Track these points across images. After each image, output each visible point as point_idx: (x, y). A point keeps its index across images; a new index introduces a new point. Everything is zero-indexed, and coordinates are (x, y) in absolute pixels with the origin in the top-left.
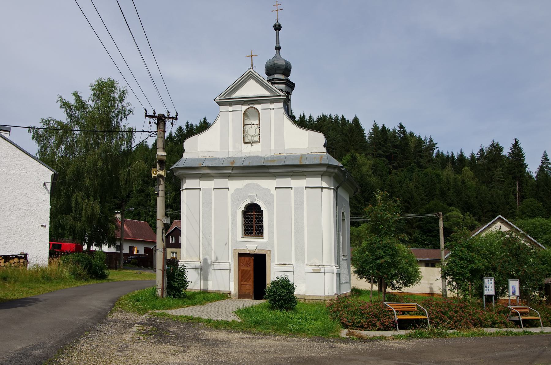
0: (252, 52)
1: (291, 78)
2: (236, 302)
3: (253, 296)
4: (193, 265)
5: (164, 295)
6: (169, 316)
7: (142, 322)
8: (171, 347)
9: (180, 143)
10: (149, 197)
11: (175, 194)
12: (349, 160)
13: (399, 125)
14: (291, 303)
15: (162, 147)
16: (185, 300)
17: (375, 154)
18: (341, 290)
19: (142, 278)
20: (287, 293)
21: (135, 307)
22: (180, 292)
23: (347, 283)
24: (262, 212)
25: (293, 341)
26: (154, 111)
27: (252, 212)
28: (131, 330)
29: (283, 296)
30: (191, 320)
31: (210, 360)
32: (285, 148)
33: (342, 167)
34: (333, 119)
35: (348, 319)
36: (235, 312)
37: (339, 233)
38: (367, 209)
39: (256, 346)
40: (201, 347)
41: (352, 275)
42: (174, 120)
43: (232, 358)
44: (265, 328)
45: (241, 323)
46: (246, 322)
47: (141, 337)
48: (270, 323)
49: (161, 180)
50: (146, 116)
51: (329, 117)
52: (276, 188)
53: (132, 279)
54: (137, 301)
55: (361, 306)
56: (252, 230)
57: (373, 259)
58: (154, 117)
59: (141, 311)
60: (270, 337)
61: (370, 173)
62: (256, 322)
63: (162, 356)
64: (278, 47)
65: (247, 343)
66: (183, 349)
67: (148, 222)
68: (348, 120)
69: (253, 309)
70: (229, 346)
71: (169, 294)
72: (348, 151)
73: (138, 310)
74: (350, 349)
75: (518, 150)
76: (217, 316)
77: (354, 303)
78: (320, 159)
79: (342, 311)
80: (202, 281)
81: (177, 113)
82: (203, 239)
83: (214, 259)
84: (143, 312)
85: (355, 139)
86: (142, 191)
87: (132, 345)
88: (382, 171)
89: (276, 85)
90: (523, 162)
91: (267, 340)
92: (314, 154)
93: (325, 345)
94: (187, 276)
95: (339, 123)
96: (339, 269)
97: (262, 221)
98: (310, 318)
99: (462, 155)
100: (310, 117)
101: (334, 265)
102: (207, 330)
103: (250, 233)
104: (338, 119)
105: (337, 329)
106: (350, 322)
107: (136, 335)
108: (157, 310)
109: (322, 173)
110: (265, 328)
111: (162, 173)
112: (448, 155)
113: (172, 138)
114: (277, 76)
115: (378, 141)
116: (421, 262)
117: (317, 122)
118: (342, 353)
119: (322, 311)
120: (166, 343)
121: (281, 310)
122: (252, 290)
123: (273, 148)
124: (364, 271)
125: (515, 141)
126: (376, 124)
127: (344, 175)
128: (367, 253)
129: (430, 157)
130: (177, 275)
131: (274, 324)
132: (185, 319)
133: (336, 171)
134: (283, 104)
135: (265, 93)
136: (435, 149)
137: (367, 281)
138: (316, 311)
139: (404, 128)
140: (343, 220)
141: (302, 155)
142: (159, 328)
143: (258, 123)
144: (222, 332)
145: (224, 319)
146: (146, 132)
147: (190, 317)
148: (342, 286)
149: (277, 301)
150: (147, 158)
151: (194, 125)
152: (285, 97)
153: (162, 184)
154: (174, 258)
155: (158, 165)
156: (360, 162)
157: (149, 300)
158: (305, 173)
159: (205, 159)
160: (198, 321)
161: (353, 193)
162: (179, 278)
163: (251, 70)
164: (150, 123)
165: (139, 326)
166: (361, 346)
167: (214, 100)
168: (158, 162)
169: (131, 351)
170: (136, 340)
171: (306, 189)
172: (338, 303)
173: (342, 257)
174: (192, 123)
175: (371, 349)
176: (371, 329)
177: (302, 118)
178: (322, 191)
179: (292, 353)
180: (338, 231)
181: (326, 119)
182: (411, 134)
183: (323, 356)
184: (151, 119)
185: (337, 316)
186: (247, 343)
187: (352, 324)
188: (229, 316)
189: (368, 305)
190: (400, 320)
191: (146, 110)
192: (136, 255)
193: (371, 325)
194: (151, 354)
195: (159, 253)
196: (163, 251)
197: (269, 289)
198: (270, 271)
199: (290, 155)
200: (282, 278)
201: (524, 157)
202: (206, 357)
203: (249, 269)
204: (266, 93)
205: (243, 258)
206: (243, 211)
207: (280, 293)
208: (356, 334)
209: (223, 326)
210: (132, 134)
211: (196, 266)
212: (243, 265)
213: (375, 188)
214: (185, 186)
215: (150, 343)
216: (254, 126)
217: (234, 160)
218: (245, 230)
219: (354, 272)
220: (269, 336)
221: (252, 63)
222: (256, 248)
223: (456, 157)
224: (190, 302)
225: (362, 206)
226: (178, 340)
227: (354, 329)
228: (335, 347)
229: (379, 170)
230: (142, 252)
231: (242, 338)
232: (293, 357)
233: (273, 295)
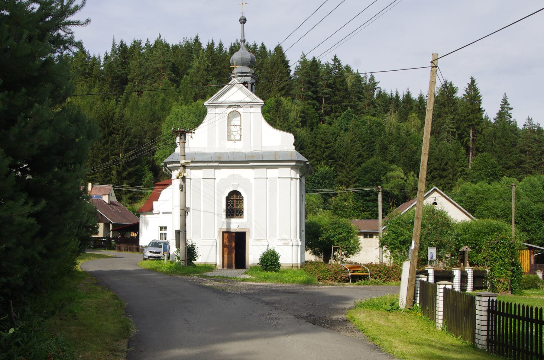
13: (333, 58)
24: (243, 197)
33: (307, 162)
75: (474, 91)
90: (479, 106)
92: (285, 151)
99: (408, 95)
100: (221, 45)
104: (257, 48)
109: (292, 166)
112: (392, 95)
116: (360, 233)
125: (472, 81)
129: (370, 100)
133: (302, 164)
136: (376, 89)
139: (339, 61)
141: (276, 152)
182: (348, 69)
190: (352, 276)
198: (248, 245)
201: (481, 100)
217: (220, 155)
223: (401, 98)
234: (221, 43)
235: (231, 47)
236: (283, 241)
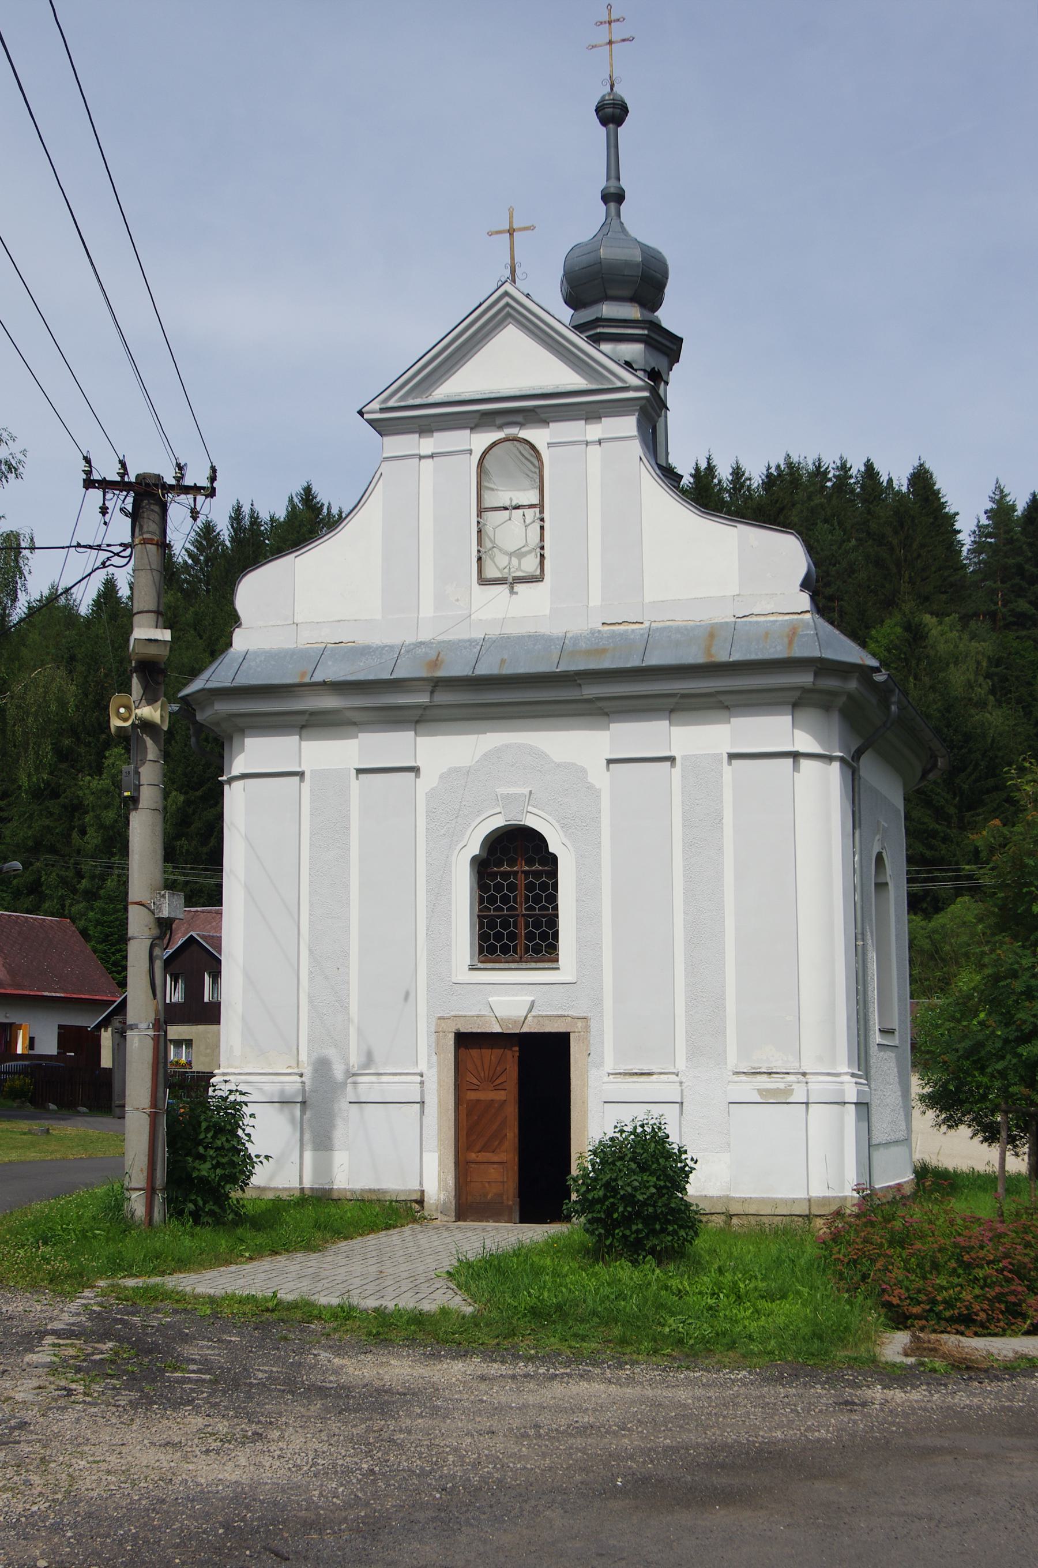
0: (511, 217)
1: (668, 316)
2: (445, 1234)
3: (517, 1208)
4: (271, 1088)
5: (157, 1216)
6: (180, 1297)
7: (73, 1324)
8: (199, 1421)
9: (208, 591)
10: (76, 814)
11: (182, 798)
12: (897, 642)
14: (675, 1232)
15: (153, 607)
16: (239, 1231)
17: (1000, 615)
18: (875, 1177)
19: (52, 1153)
20: (659, 1189)
21: (39, 1269)
22: (221, 1199)
23: (896, 1142)
24: (554, 859)
25: (691, 1383)
26: (123, 464)
27: (512, 862)
28: (29, 1358)
29: (644, 1204)
30: (273, 1311)
31: (365, 1466)
32: (647, 600)
33: (877, 670)
34: (830, 475)
35: (908, 1289)
36: (448, 1272)
37: (863, 940)
38: (981, 838)
39: (542, 1408)
40: (324, 1420)
41: (916, 1113)
42: (200, 499)
43: (451, 1458)
44: (576, 1335)
45: (474, 1316)
46: (494, 1314)
47: (73, 1386)
48: (594, 1313)
49: (149, 742)
50: (89, 483)
51: (811, 467)
52: (610, 762)
53: (14, 1156)
54: (45, 1243)
55: (960, 1235)
56: (513, 937)
57: (1006, 1041)
58: (121, 485)
59: (62, 1282)
60: (597, 1371)
61: (981, 691)
62: (536, 1313)
63: (168, 1457)
64: (612, 190)
65: (503, 1395)
66: (251, 1429)
67: (73, 921)
68: (890, 481)
69: (521, 1258)
70: (435, 1411)
71: (175, 1210)
72: (890, 603)
73: (51, 1281)
74: (925, 1409)
76: (379, 1293)
77: (930, 1222)
78: (786, 640)
79: (886, 1256)
80: (308, 1155)
81: (214, 470)
82: (311, 979)
83: (355, 1059)
84: (72, 1286)
85: (919, 556)
86: (52, 791)
87: (41, 1420)
88: (1030, 684)
89: (606, 347)
91: (584, 1384)
92: (762, 619)
93: (820, 1396)
94: (249, 1135)
95: (853, 491)
96: (866, 1088)
97: (553, 899)
98: (756, 1289)
100: (737, 473)
101: (846, 1070)
102: (338, 1350)
103: (505, 950)
104: (851, 477)
105: (868, 1332)
106: (919, 1303)
107: (52, 1379)
108: (132, 1275)
110: (576, 1335)
111: (150, 712)
113: (173, 573)
114: (608, 310)
115: (1011, 561)
117: (765, 489)
118: (893, 1424)
119: (802, 1261)
120: (176, 1405)
121: (637, 1261)
122: (512, 1186)
123: (595, 600)
124: (962, 1096)
126: (1002, 491)
127: (885, 703)
128: (982, 1015)
130: (207, 1130)
131: (609, 1319)
132: (247, 1308)
133: (853, 685)
134: (639, 422)
135: (567, 378)
137: (975, 1135)
138: (778, 1262)
140: (881, 886)
142: (143, 1349)
143: (535, 501)
144: (400, 1357)
145: (408, 1302)
146: (90, 547)
147: (266, 1300)
148: (878, 1156)
149: (617, 1224)
150: (72, 658)
151: (264, 516)
152: (646, 394)
153: (151, 756)
154: (183, 1066)
155: (135, 681)
156: (942, 647)
157: (95, 1236)
158: (727, 699)
159: (322, 653)
160: (299, 1315)
161: (919, 774)
162: (219, 1143)
163: (508, 287)
164: (104, 510)
165: (61, 1342)
166: (968, 1396)
167: (361, 413)
168: (136, 670)
169: (39, 1441)
170: (56, 1400)
171: (730, 764)
172: (865, 1225)
173: (877, 1038)
174: (257, 508)
175: (1010, 1409)
176: (1004, 1330)
177: (704, 476)
178: (796, 768)
179: (690, 1431)
180: (859, 931)
181: (801, 476)
183: (818, 1440)
184: (109, 496)
185: (864, 1277)
186: (503, 1395)
187: (924, 1311)
188: (425, 1290)
189: (991, 1230)
191: (87, 460)
192: (22, 1057)
193: (1002, 1312)
194: (124, 1450)
195: (136, 1040)
196: (151, 1033)
197: (586, 1176)
199: (664, 629)
200: (639, 1130)
202: (345, 1456)
203: (500, 1096)
204: (572, 380)
205: (474, 1052)
206: (474, 859)
207: (629, 1189)
208: (944, 1349)
209: (404, 1333)
210: (16, 561)
211: (282, 1092)
212: (475, 1081)
213: (1000, 754)
214: (238, 765)
215: (114, 1409)
216: (520, 512)
218: (483, 937)
219: (922, 1098)
220: (593, 1365)
221: (512, 258)
222: (530, 1010)
224: (261, 1239)
225: (949, 826)
226: (224, 1392)
227: (934, 1331)
228: (864, 1404)
229: (1017, 678)
230: (48, 1046)
231: (483, 1378)
232: (698, 1445)
233: (601, 1201)
234: (738, 468)
235: (767, 477)
236: (759, 1078)
